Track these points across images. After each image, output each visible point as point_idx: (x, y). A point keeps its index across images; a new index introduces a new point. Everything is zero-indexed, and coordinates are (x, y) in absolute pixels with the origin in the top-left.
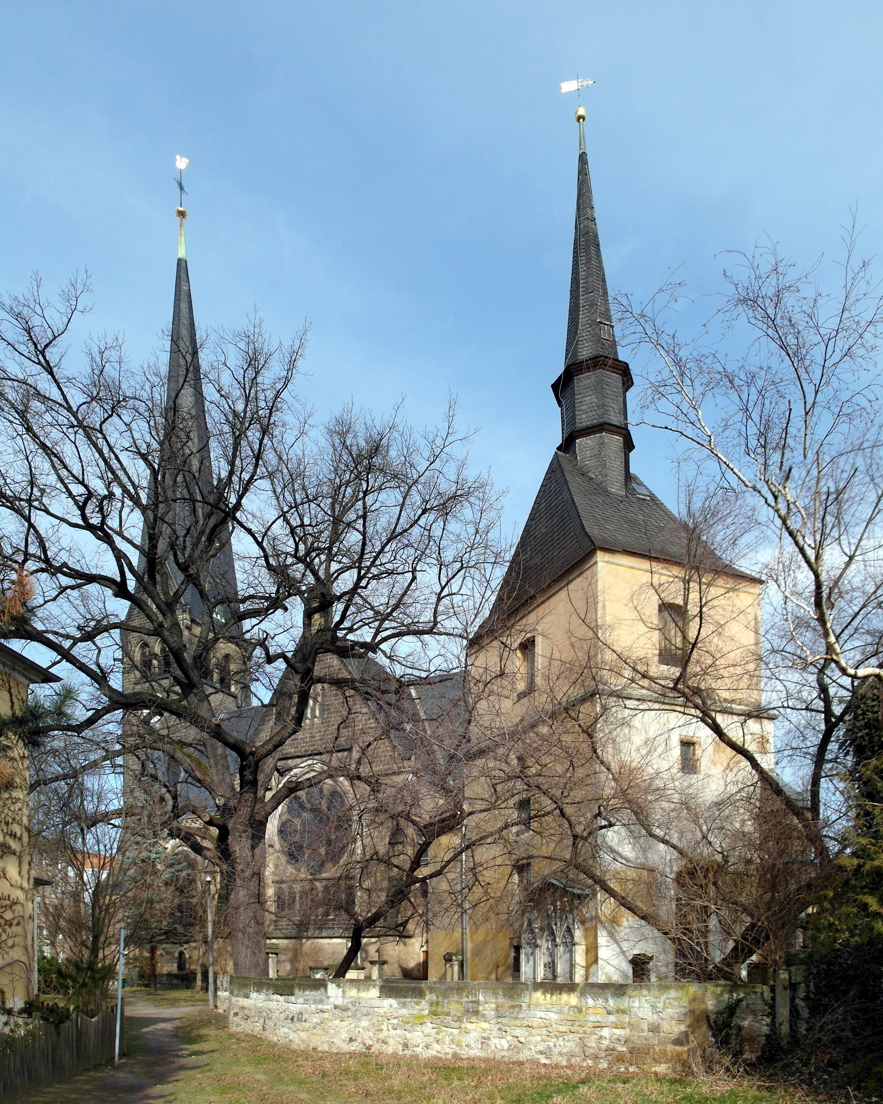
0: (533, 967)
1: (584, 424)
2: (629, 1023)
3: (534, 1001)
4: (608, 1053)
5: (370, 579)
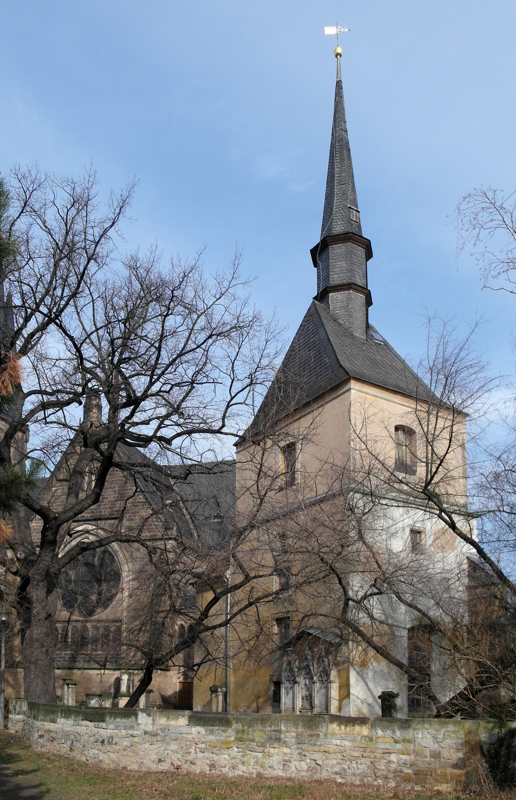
0: (293, 698)
1: (336, 282)
2: (414, 750)
3: (330, 730)
4: (396, 774)
5: (173, 385)
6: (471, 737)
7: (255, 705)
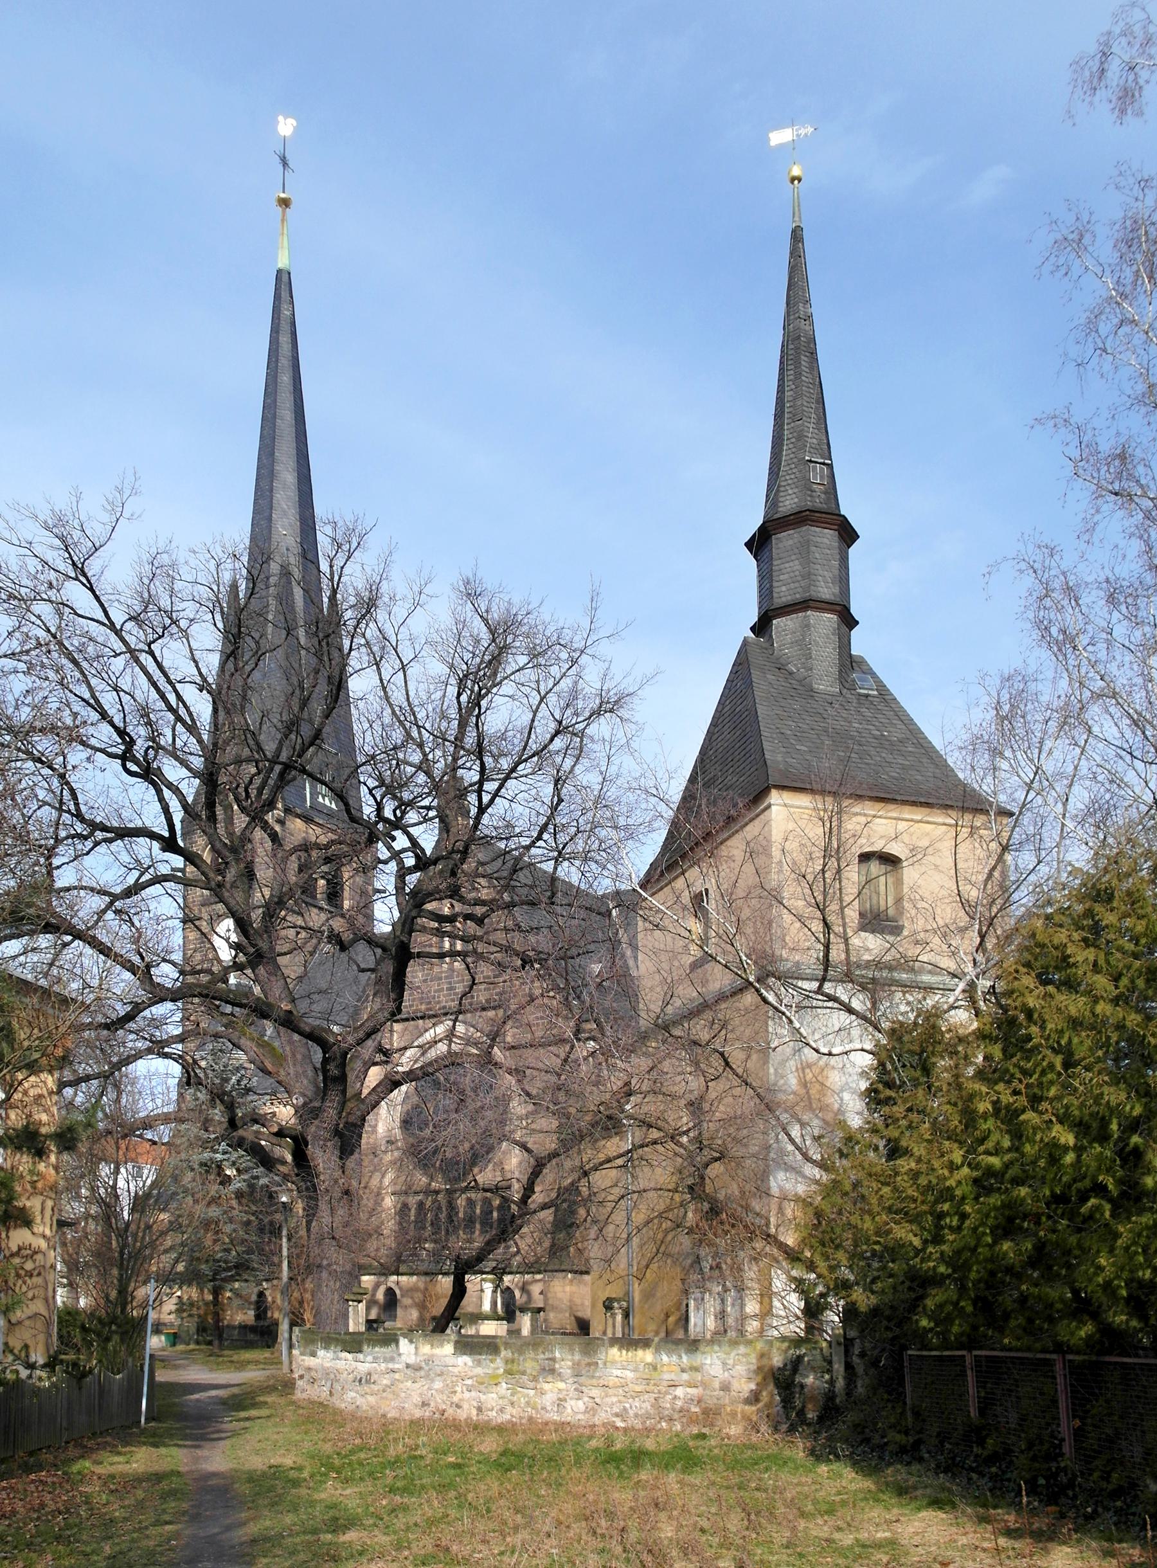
1: (784, 599)
2: (702, 1382)
6: (765, 1361)
7: (664, 1329)
